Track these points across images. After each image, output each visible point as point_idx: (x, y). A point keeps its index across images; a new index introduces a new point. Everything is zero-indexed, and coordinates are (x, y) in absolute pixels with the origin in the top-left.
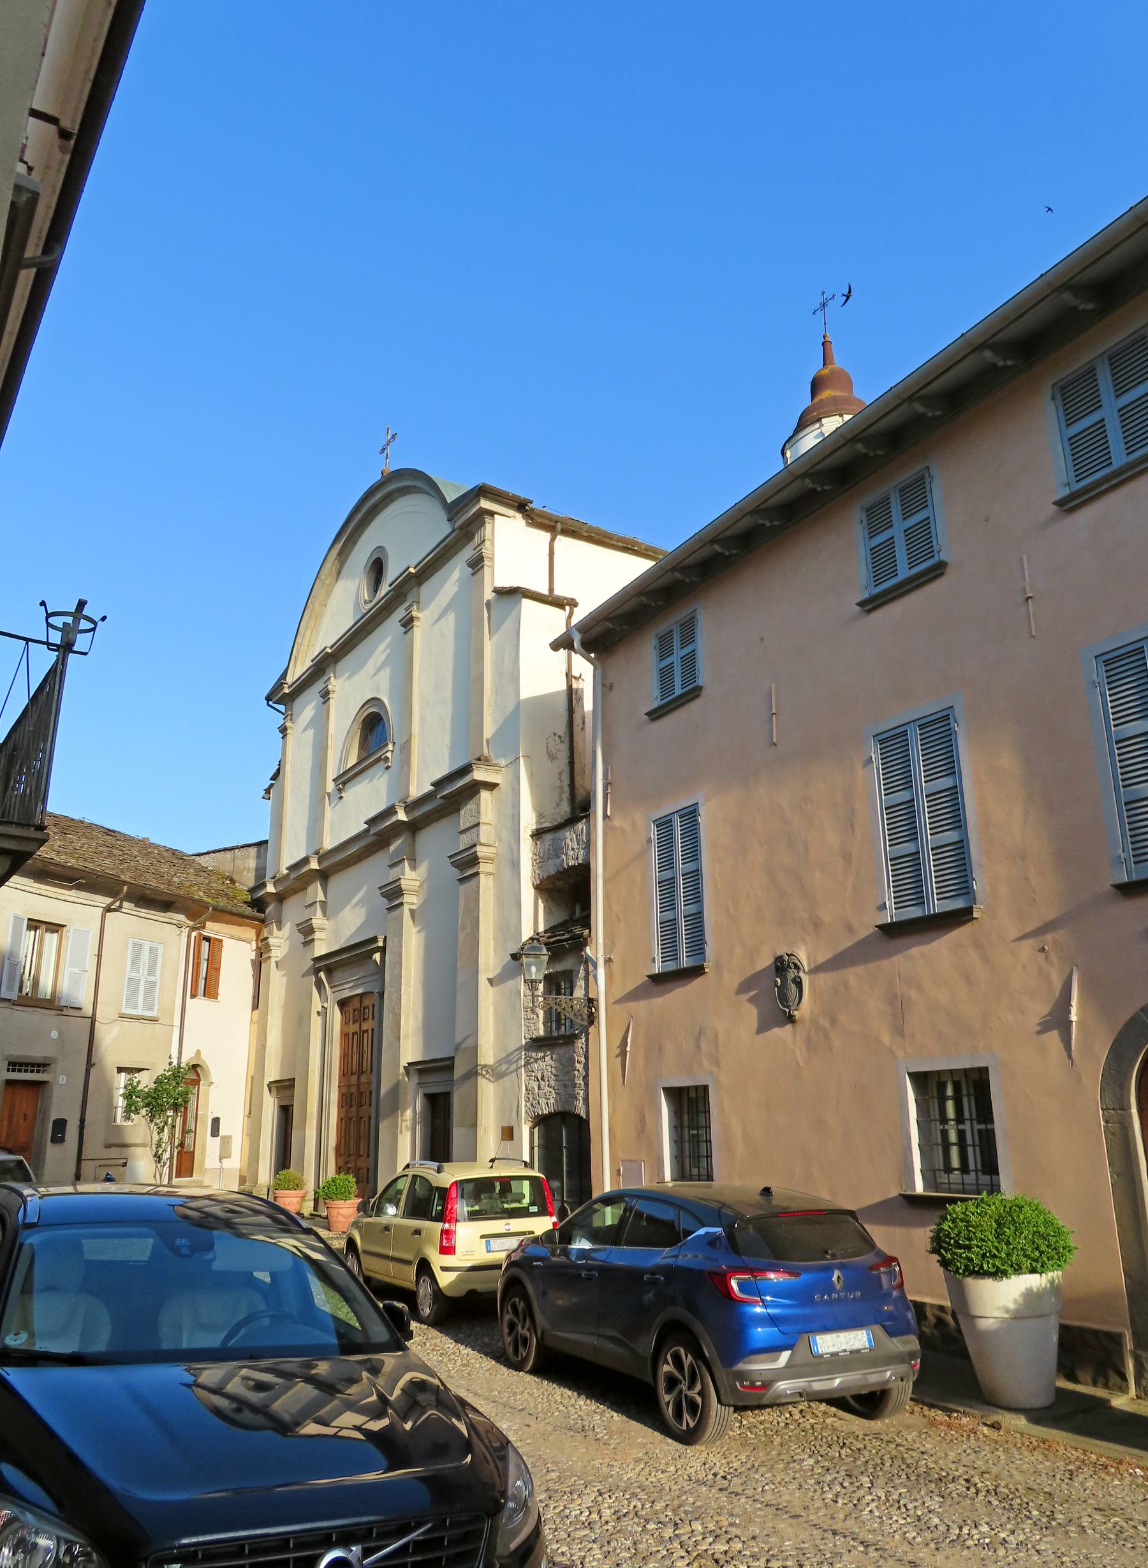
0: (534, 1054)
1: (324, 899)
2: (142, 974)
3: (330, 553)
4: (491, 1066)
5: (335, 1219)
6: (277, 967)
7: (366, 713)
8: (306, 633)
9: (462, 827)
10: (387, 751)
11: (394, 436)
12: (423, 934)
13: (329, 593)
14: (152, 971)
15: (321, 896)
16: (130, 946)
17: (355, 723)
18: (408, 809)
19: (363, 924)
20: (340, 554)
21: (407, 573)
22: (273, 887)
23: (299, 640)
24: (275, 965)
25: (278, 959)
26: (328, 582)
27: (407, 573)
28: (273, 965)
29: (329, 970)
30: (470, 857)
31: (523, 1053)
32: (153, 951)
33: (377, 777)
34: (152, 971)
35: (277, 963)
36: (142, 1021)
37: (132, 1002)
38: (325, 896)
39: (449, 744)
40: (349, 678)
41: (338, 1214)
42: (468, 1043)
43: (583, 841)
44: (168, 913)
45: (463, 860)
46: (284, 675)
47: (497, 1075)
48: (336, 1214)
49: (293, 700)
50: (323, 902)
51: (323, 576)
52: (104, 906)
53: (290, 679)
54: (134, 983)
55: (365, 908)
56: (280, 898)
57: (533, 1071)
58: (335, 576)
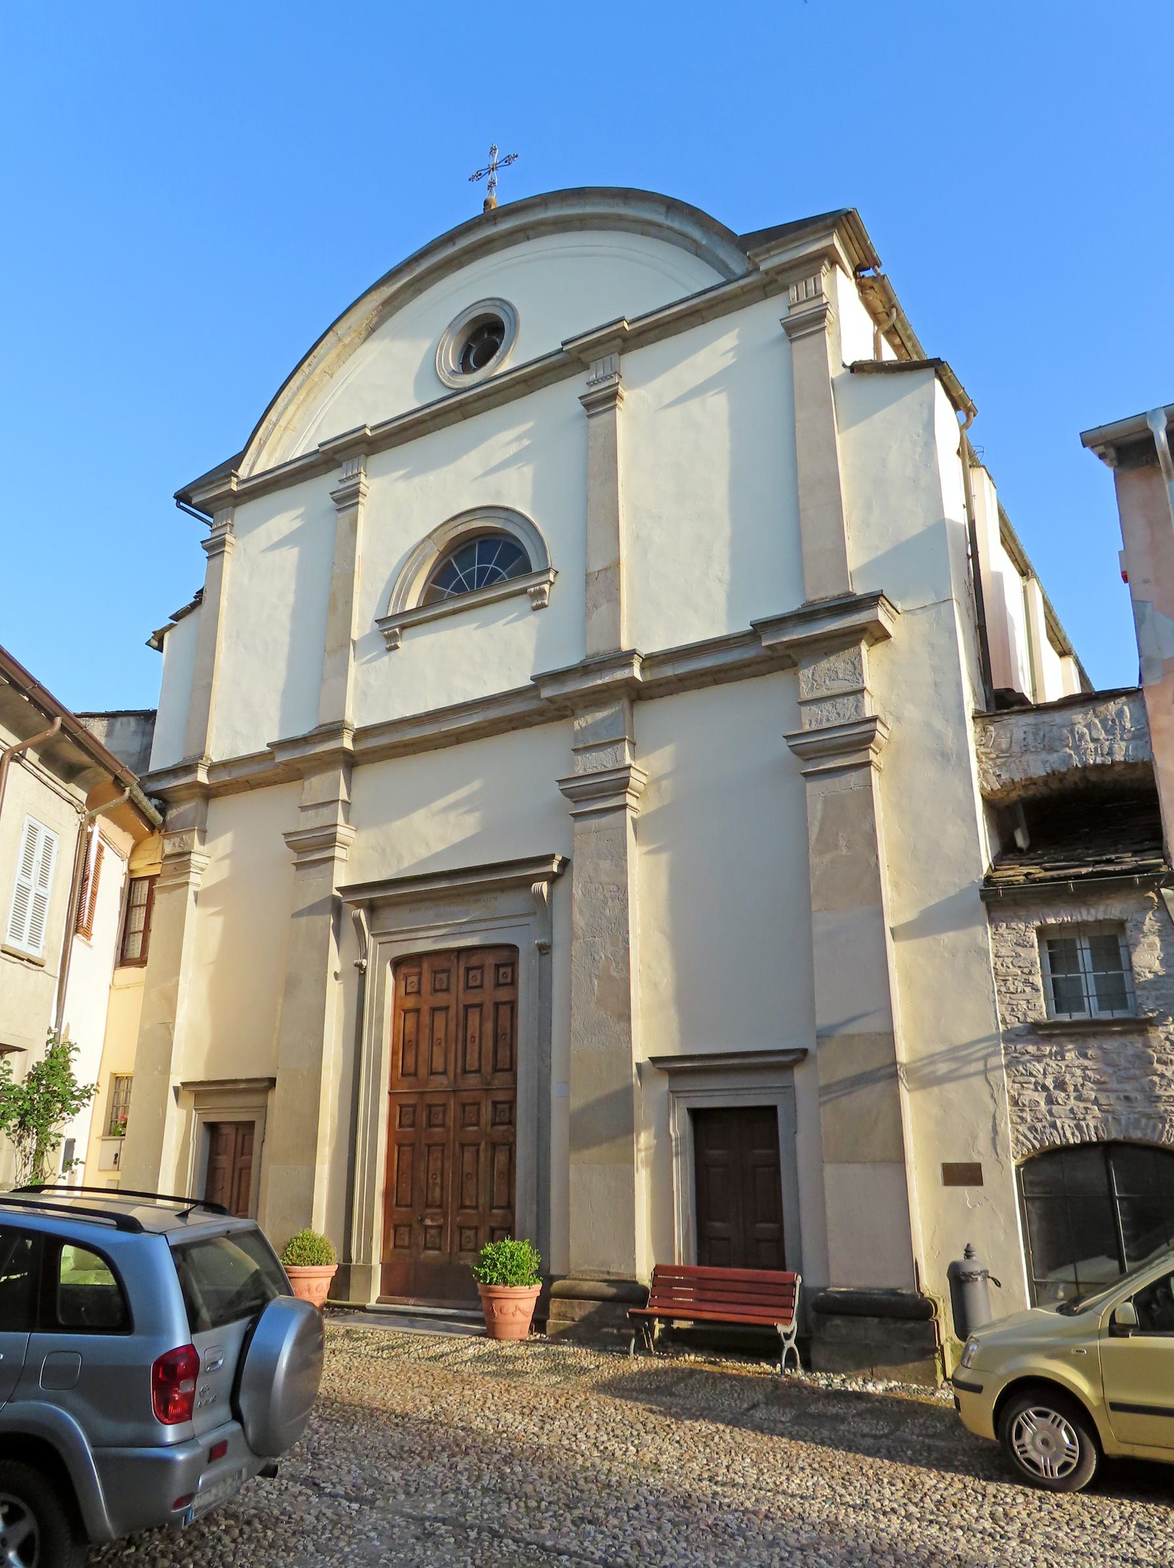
0: (1031, 1049)
1: (347, 799)
2: (32, 882)
3: (369, 298)
4: (905, 1065)
5: (509, 1318)
6: (196, 901)
7: (462, 529)
8: (288, 411)
9: (806, 695)
10: (545, 582)
11: (508, 160)
12: (664, 858)
13: (341, 359)
14: (43, 883)
15: (343, 795)
16: (26, 827)
17: (430, 542)
18: (647, 663)
19: (473, 837)
20: (386, 303)
21: (615, 327)
22: (205, 776)
23: (272, 415)
24: (193, 898)
25: (197, 889)
26: (347, 340)
27: (615, 327)
28: (191, 897)
29: (372, 908)
30: (851, 739)
31: (1002, 1046)
32: (49, 841)
33: (505, 621)
34: (43, 883)
35: (196, 894)
36: (25, 963)
37: (16, 933)
38: (349, 795)
39: (726, 577)
40: (406, 477)
41: (517, 1308)
42: (870, 1025)
43: (1123, 728)
44: (72, 785)
45: (827, 742)
46: (237, 460)
47: (926, 1081)
48: (512, 1309)
49: (236, 505)
50: (347, 802)
51: (341, 328)
52: (7, 748)
53: (243, 472)
54: (23, 891)
55: (477, 814)
56: (208, 794)
57: (1031, 1074)
58: (364, 333)
